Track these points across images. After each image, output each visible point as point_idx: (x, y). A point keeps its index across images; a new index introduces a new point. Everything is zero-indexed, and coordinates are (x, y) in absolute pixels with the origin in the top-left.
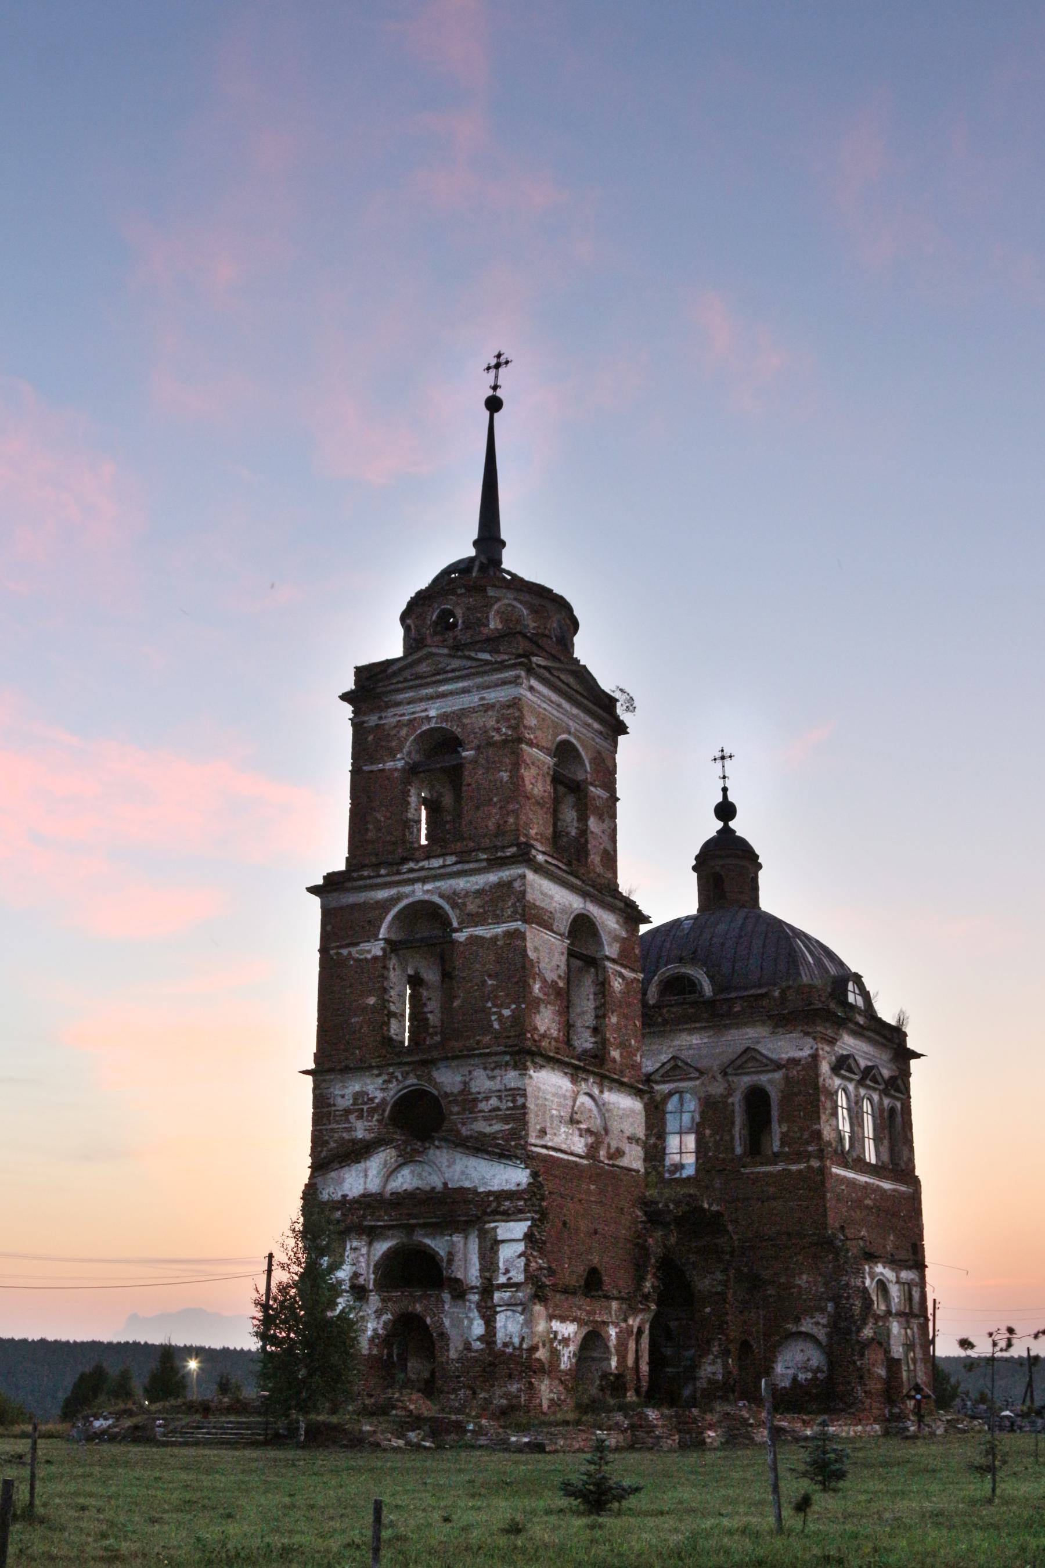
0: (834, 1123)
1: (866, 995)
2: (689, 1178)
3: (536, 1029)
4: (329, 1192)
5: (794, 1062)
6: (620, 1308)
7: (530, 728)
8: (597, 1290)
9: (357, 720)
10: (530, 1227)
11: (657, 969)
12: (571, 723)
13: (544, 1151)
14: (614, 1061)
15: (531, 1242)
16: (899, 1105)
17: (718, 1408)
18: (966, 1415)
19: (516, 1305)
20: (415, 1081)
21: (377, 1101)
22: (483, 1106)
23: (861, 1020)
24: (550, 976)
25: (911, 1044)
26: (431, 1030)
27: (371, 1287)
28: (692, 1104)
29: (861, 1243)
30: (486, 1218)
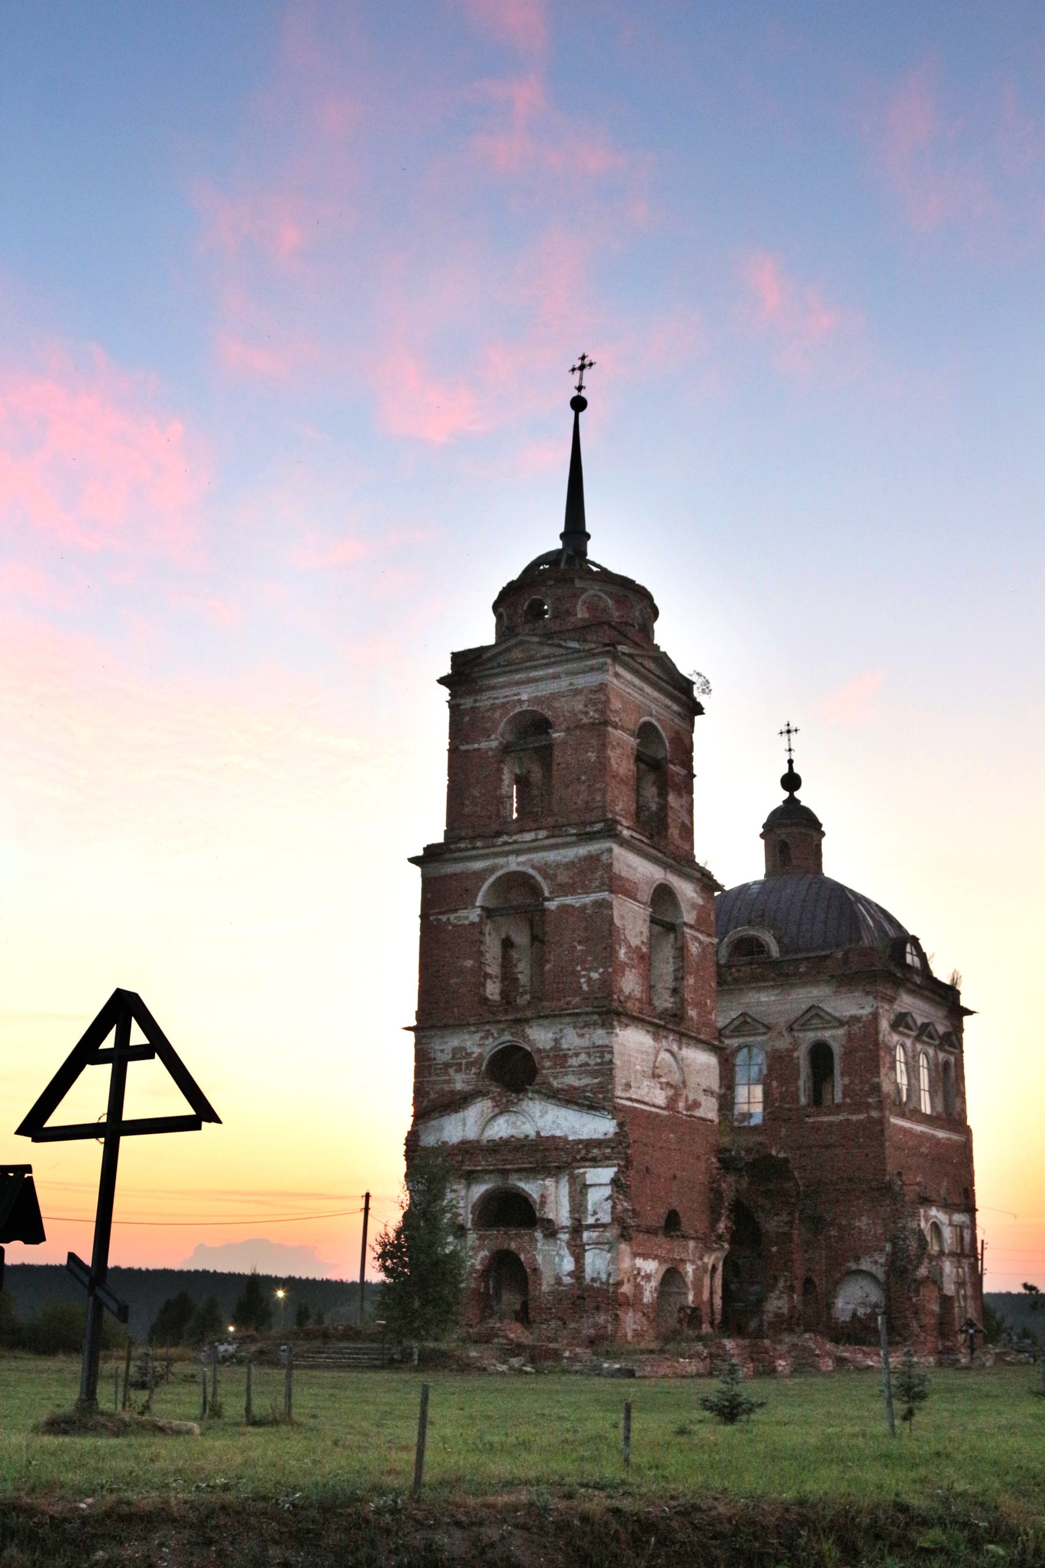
0: (892, 1077)
1: (922, 956)
2: (756, 1127)
3: (621, 991)
4: (429, 1140)
5: (855, 1019)
6: (696, 1247)
7: (616, 711)
8: (675, 1231)
9: (453, 702)
10: (616, 1173)
11: (727, 932)
12: (653, 706)
13: (629, 1103)
14: (692, 1019)
15: (618, 1186)
16: (952, 1059)
17: (787, 1340)
18: (1012, 1348)
19: (602, 1244)
20: (510, 1038)
21: (475, 1055)
22: (574, 1061)
23: (918, 980)
24: (635, 942)
25: (964, 1002)
26: (521, 990)
27: (469, 1225)
28: (760, 1058)
29: (916, 1187)
30: (575, 1164)
